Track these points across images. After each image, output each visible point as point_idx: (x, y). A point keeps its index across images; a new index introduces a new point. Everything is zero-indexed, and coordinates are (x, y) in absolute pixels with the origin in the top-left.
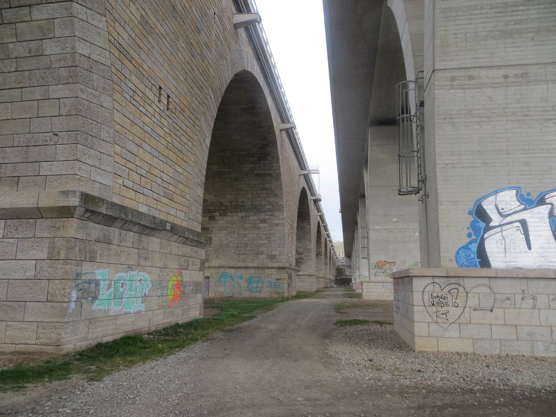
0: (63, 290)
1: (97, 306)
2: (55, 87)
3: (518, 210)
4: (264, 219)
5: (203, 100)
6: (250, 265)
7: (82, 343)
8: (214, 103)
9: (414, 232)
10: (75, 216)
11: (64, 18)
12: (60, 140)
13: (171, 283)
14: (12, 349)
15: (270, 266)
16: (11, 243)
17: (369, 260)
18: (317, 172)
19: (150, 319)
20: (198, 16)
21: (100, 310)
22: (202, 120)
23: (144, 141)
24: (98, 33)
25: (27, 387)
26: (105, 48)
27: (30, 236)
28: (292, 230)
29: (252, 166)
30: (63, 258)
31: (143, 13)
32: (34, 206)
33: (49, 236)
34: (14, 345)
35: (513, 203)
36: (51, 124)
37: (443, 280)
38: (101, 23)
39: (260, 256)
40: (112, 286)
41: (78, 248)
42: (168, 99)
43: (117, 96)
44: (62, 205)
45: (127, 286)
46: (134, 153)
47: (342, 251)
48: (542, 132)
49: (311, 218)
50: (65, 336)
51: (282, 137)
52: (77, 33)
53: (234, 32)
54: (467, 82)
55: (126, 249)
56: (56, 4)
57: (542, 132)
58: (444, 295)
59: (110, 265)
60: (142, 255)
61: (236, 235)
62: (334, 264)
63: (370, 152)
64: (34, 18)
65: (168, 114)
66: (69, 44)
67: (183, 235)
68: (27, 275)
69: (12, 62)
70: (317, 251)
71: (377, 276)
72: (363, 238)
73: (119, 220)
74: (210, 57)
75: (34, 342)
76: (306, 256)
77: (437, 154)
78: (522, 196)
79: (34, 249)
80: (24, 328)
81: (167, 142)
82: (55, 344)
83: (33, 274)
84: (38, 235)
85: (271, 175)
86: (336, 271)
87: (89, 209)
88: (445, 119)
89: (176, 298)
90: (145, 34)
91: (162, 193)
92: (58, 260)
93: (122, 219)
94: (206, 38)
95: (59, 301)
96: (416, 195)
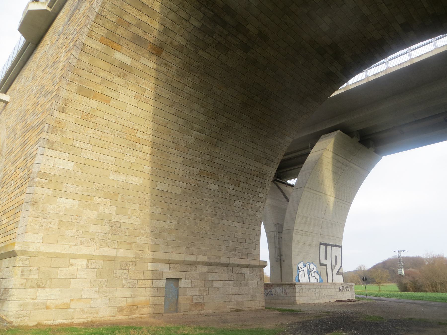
33: (259, 274)
54: (298, 233)
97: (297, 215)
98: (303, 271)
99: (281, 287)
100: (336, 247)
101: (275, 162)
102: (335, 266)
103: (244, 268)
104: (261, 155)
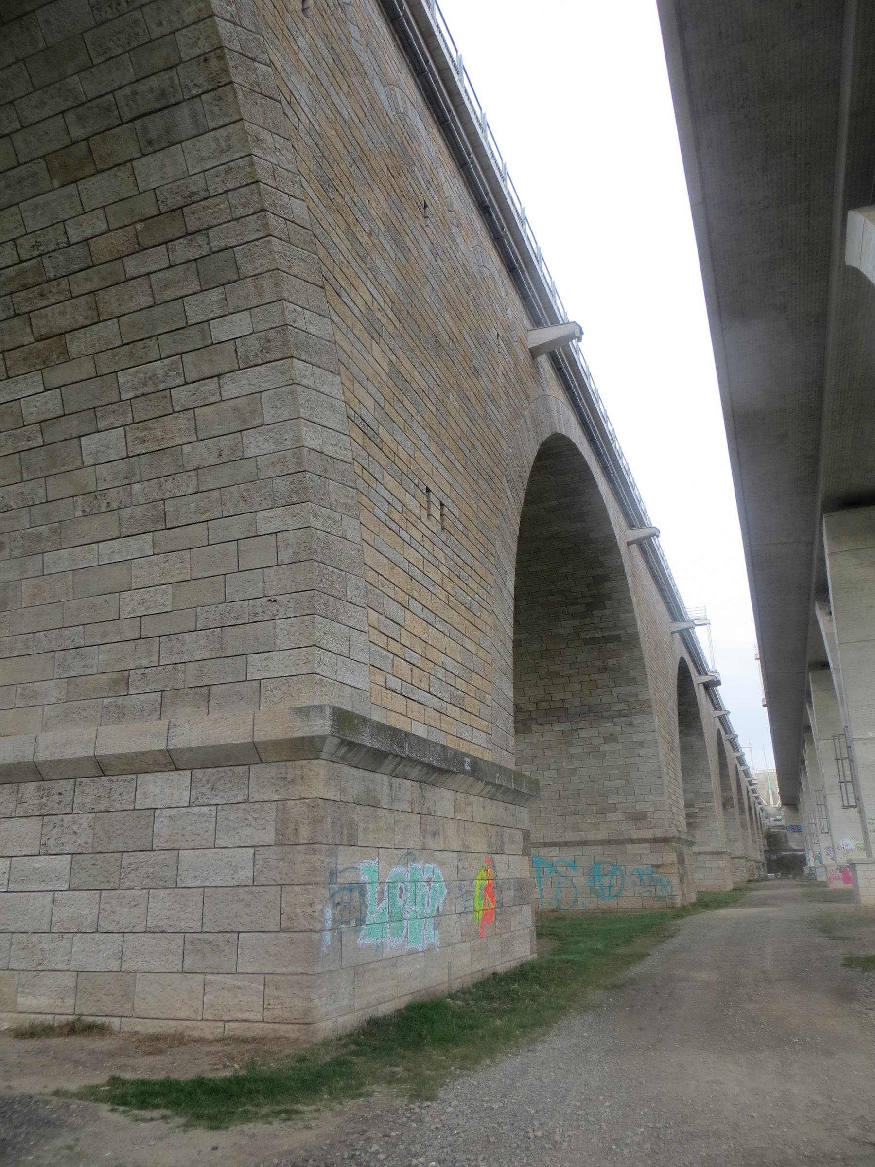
0: (311, 905)
1: (364, 938)
2: (267, 514)
4: (612, 735)
5: (495, 503)
6: (591, 836)
7: (345, 1018)
8: (514, 506)
10: (324, 755)
11: (280, 389)
12: (282, 610)
13: (478, 883)
14: (218, 1033)
15: (634, 837)
16: (203, 815)
17: (861, 812)
18: (705, 622)
19: (449, 963)
20: (473, 346)
21: (369, 947)
22: (498, 543)
23: (412, 597)
24: (332, 406)
25: (303, 1112)
26: (343, 431)
27: (240, 799)
28: (672, 754)
29: (576, 622)
30: (306, 841)
31: (393, 358)
32: (246, 741)
33: (275, 797)
34: (221, 1024)
36: (264, 582)
38: (332, 386)
39: (612, 817)
40: (386, 894)
41: (329, 820)
42: (441, 510)
43: (365, 515)
45: (409, 894)
46: (398, 622)
47: (773, 793)
49: (703, 724)
50: (320, 1004)
51: (632, 558)
52: (303, 412)
53: (531, 363)
55: (403, 816)
56: (264, 365)
59: (380, 850)
60: (428, 827)
61: (554, 773)
62: (760, 826)
63: (831, 568)
64: (225, 396)
65: (444, 539)
66: (290, 432)
67: (492, 781)
68: (238, 879)
69: (189, 477)
70: (723, 797)
72: (840, 761)
73: (391, 757)
74: (499, 418)
75: (260, 1017)
76: (701, 809)
79: (249, 825)
80: (239, 988)
81: (447, 594)
82: (301, 1021)
83: (251, 875)
84: (255, 796)
85: (617, 638)
86: (765, 841)
87: (345, 740)
89: (488, 917)
90: (397, 395)
91: (447, 697)
92: (296, 844)
93: (396, 756)
94: (489, 384)
95: (304, 928)
101: (194, 92)
103: (150, 777)
104: (77, 132)
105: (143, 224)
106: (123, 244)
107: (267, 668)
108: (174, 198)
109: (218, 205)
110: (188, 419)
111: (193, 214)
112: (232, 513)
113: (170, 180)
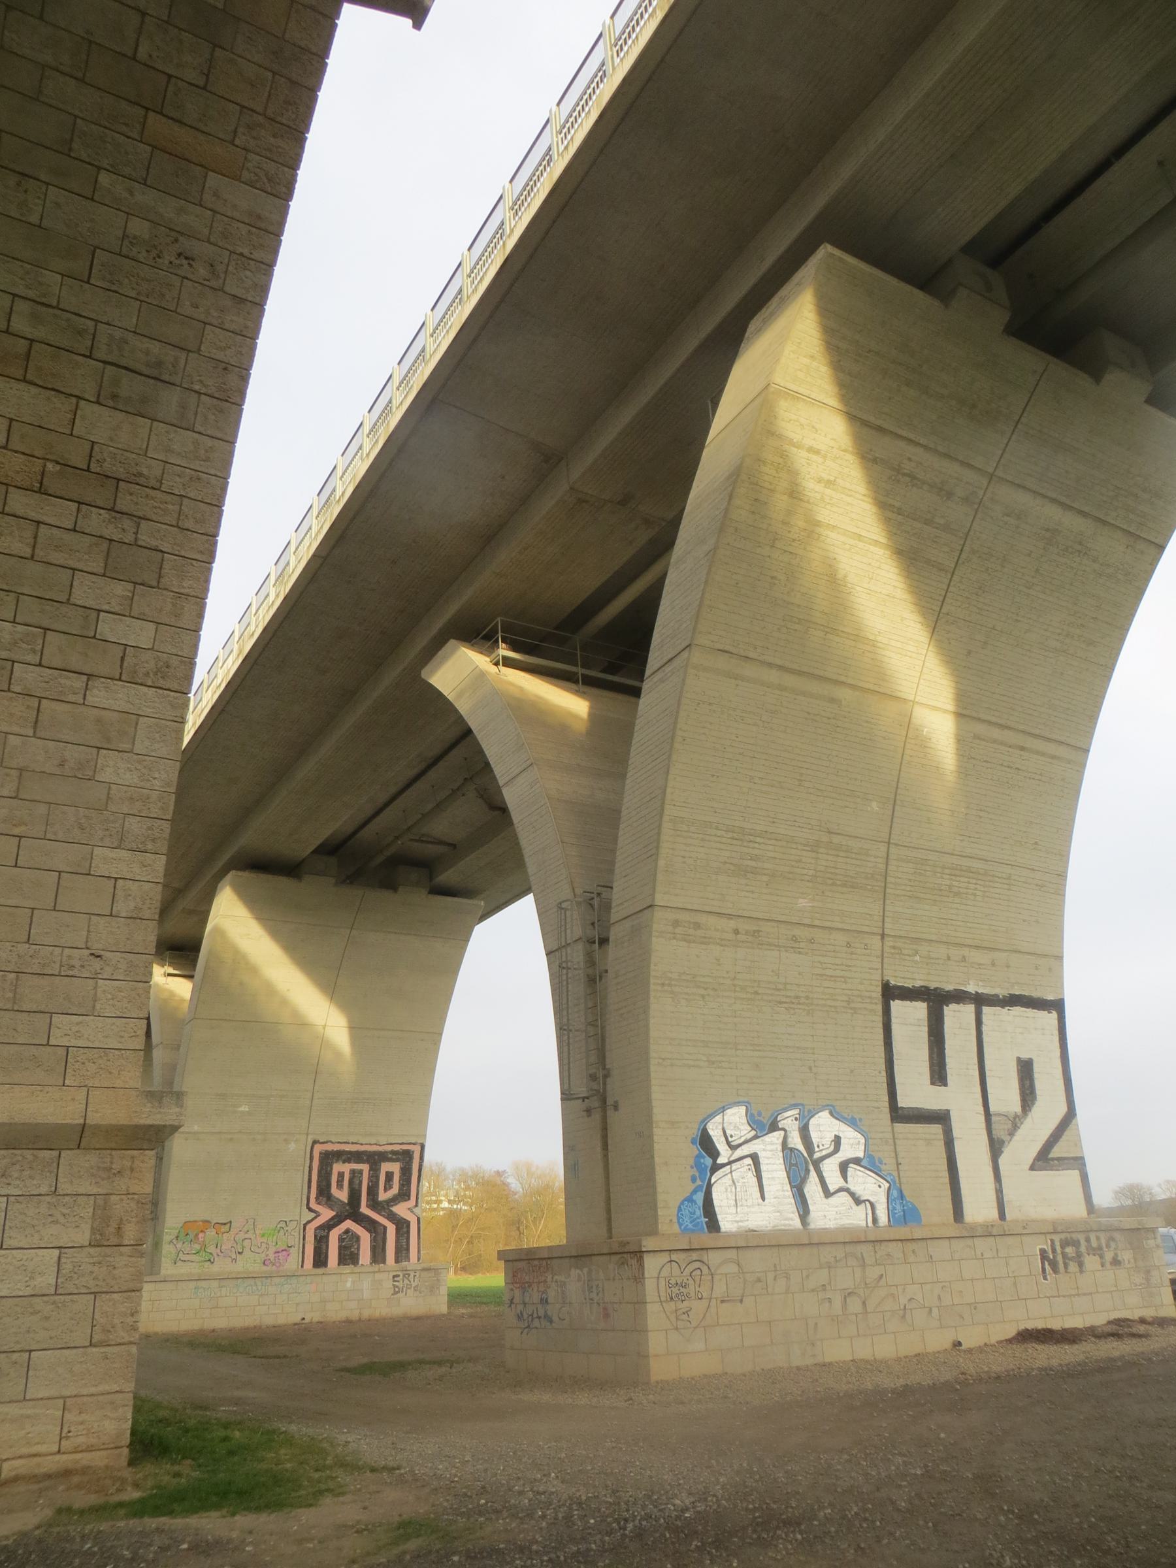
3: (748, 1138)
9: (286, 1140)
11: (163, 722)
27: (44, 1189)
30: (132, 1242)
32: (77, 1122)
33: (95, 1190)
35: (742, 1127)
36: (88, 931)
37: (682, 1256)
44: (149, 1122)
48: (773, 1020)
54: (691, 931)
56: (154, 689)
57: (773, 1020)
58: (685, 1281)
64: (90, 699)
69: (7, 775)
71: (179, 1263)
77: (651, 1041)
78: (752, 1115)
79: (56, 1222)
80: (28, 1417)
82: (112, 1446)
88: (663, 985)
96: (583, 1101)
97: (665, 818)
98: (749, 1161)
99: (585, 1270)
100: (1018, 1010)
101: (197, 387)
102: (1015, 1124)
105: (58, 467)
106: (18, 472)
107: (78, 1034)
108: (114, 465)
109: (166, 503)
110: (28, 707)
111: (131, 494)
112: (60, 836)
113: (120, 446)
